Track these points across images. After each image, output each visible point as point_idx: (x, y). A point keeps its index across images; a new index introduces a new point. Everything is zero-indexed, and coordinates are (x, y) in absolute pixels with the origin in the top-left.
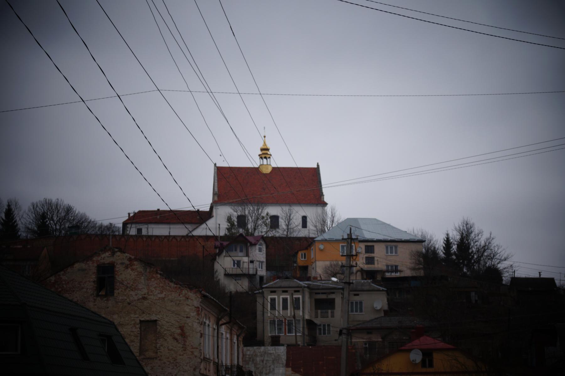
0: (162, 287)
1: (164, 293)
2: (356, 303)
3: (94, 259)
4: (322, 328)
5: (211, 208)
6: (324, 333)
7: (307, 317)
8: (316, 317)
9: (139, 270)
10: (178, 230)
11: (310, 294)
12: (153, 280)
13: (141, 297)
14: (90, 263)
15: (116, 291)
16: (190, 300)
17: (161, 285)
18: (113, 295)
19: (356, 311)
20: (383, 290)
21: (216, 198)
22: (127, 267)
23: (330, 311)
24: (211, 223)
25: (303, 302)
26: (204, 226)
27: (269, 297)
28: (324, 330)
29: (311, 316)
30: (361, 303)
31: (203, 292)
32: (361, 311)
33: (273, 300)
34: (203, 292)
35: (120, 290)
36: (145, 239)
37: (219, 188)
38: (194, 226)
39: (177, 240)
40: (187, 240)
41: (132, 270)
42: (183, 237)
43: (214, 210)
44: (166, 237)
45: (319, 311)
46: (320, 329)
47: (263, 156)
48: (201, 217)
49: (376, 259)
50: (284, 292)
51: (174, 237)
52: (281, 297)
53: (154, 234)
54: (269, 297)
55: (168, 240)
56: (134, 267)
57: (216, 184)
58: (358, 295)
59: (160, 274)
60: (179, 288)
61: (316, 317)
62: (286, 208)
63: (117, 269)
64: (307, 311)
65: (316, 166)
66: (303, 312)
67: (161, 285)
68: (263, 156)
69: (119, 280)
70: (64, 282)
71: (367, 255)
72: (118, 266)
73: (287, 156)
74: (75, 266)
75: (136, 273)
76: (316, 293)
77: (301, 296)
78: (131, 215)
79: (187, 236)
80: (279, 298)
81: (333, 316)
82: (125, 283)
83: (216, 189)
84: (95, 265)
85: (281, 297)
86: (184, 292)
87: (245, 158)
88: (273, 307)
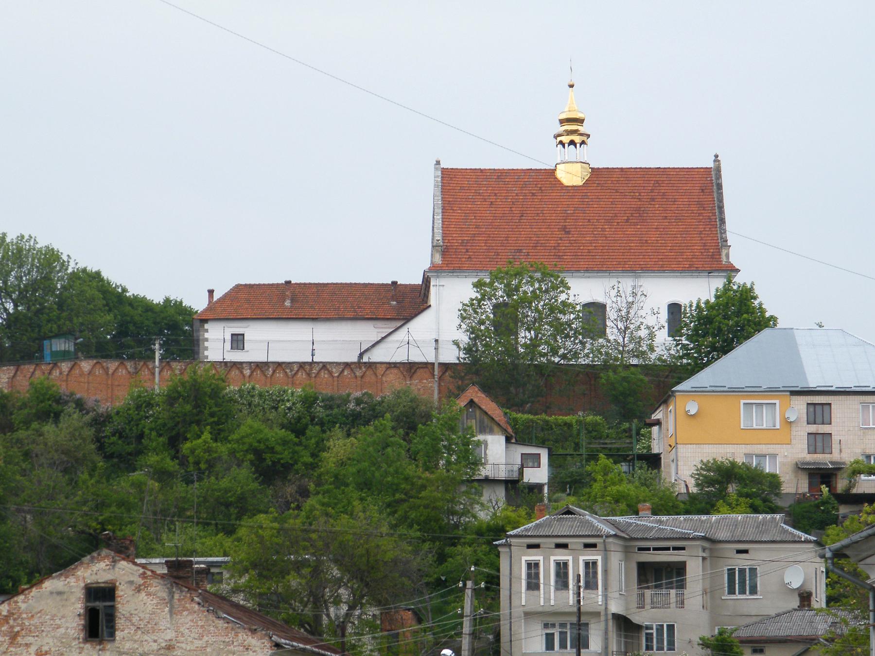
0: (202, 626)
1: (206, 638)
2: (742, 571)
3: (79, 573)
4: (654, 632)
5: (426, 281)
6: (660, 648)
7: (615, 608)
8: (641, 606)
9: (160, 594)
10: (334, 343)
11: (627, 551)
12: (185, 613)
13: (163, 645)
14: (72, 580)
15: (119, 635)
16: (251, 652)
17: (200, 623)
18: (114, 640)
19: (742, 592)
20: (807, 541)
21: (438, 259)
22: (138, 590)
23: (673, 592)
24: (421, 328)
25: (606, 571)
26: (402, 335)
27: (524, 558)
28: (660, 641)
29: (627, 609)
30: (753, 571)
31: (275, 638)
32: (753, 591)
33: (533, 566)
34: (275, 638)
35: (126, 632)
36: (247, 372)
37: (445, 227)
38: (382, 329)
39: (331, 373)
40: (359, 373)
41: (149, 594)
42: (347, 365)
43: (433, 290)
44: (302, 365)
45: (648, 593)
46: (649, 637)
47: (566, 139)
48: (404, 303)
49: (835, 438)
50: (559, 546)
51: (324, 366)
52: (552, 558)
53: (272, 359)
54: (524, 558)
55: (309, 375)
56: (152, 589)
57: (439, 217)
58: (746, 551)
59: (199, 604)
60: (232, 629)
61: (641, 606)
62: (627, 284)
63: (121, 593)
64: (614, 594)
65: (710, 164)
66: (606, 597)
67: (200, 623)
68: (566, 139)
69: (124, 612)
70: (24, 616)
71: (813, 428)
72: (121, 587)
73: (634, 140)
74: (44, 586)
75: (155, 601)
76: (640, 549)
77: (599, 558)
78: (217, 296)
79: (359, 364)
80: (548, 561)
81: (681, 604)
82: (135, 619)
83: (439, 237)
84: (82, 585)
85: (552, 558)
86: (240, 637)
87: (520, 145)
88: (533, 585)
